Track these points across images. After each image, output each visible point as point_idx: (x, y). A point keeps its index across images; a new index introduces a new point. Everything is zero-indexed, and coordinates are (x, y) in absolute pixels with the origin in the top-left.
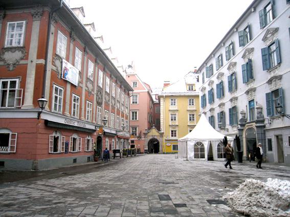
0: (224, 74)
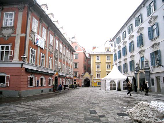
0: (126, 42)
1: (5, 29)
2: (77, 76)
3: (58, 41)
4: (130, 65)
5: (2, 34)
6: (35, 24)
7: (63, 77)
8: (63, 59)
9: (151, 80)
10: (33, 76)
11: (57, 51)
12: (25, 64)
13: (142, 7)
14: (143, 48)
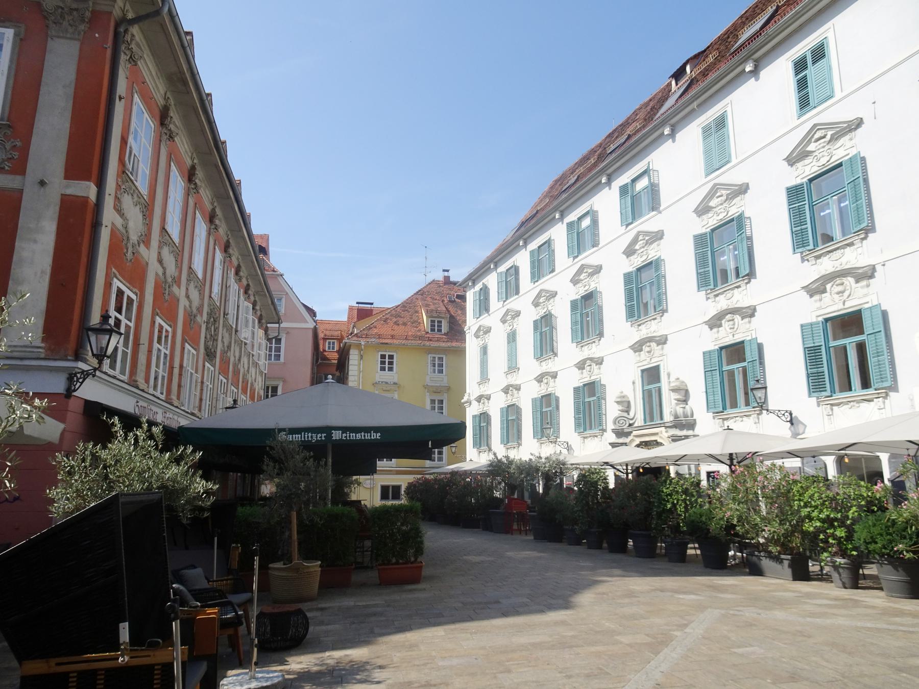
0: (556, 293)
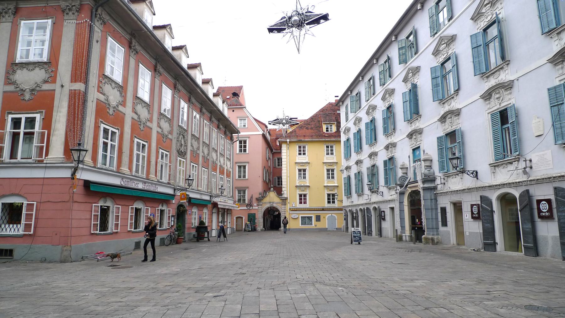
0: (376, 106)
1: (25, 69)
2: (244, 200)
3: (186, 106)
4: (386, 170)
5: (14, 83)
6: (114, 56)
7: (200, 205)
8: (201, 154)
9: (439, 210)
10: (109, 203)
11: (183, 132)
12: (83, 169)
13: (417, 10)
14: (417, 124)
